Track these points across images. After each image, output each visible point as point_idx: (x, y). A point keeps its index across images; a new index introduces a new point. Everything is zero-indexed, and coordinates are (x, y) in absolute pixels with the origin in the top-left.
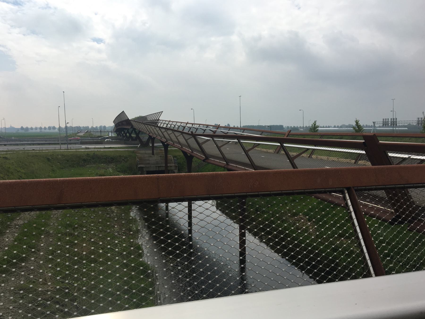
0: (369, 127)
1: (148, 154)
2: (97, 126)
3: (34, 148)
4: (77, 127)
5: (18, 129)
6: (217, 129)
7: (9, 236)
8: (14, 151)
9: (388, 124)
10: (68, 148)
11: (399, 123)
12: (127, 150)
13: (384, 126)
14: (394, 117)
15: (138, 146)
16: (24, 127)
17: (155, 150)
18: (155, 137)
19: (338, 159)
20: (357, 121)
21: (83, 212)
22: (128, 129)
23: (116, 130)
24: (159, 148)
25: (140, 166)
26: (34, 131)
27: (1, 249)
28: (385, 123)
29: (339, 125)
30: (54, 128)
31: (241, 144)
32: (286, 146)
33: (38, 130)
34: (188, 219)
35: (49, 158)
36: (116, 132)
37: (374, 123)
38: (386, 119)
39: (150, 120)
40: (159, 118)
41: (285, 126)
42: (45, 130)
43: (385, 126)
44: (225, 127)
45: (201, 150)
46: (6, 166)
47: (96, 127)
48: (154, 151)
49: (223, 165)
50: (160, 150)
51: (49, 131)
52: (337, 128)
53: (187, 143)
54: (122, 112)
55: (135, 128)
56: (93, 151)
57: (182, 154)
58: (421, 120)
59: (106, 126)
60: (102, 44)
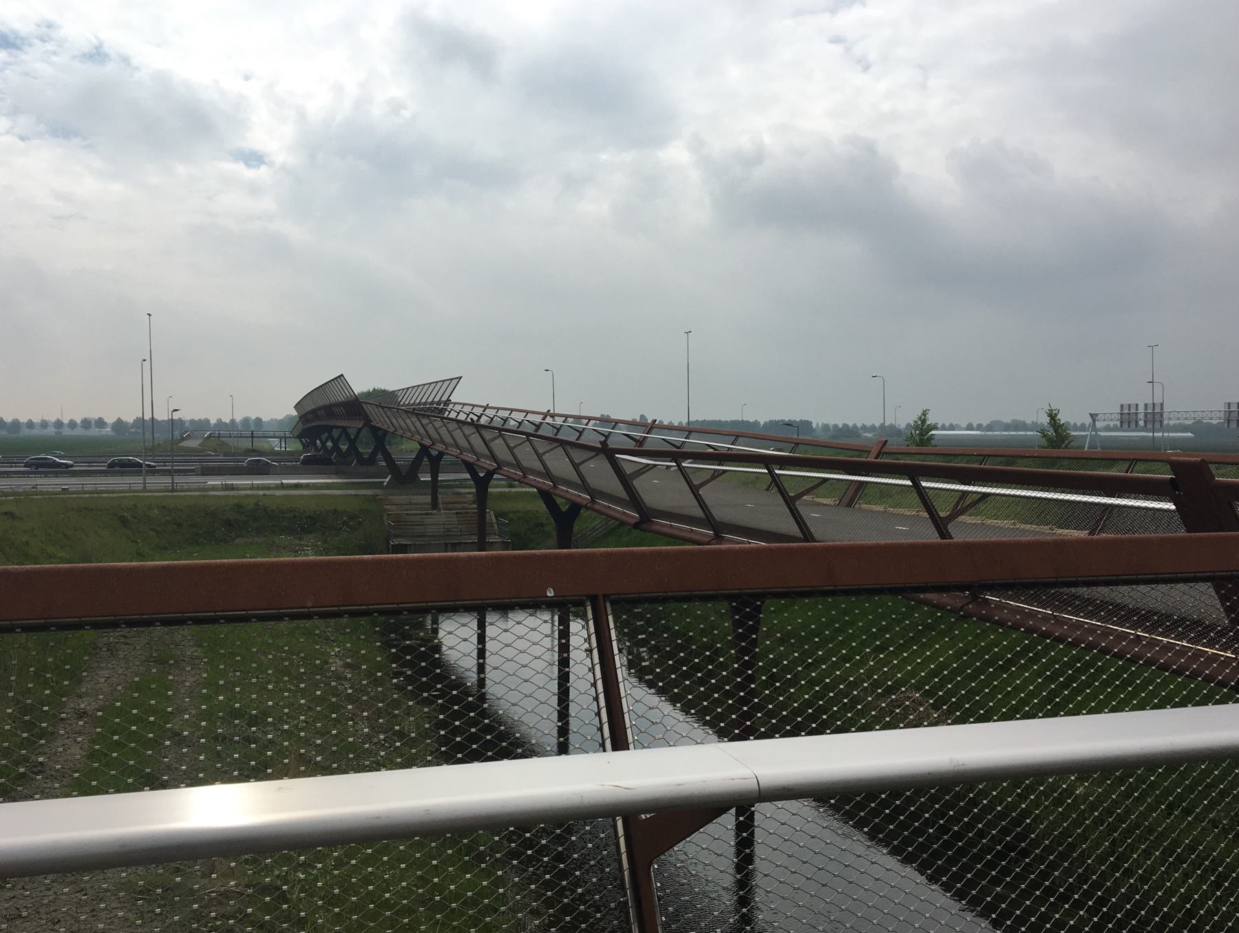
1: (420, 506)
6: (686, 438)
9: (1137, 422)
11: (1170, 419)
12: (353, 492)
13: (1125, 426)
15: (384, 482)
17: (441, 493)
19: (1014, 524)
26: (37, 432)
28: (1127, 418)
29: (1070, 421)
30: (101, 423)
31: (775, 480)
32: (928, 488)
33: (48, 428)
34: (558, 703)
35: (124, 516)
36: (299, 437)
38: (1129, 405)
40: (449, 397)
43: (1127, 427)
45: (628, 499)
48: (440, 496)
51: (71, 433)
52: (977, 430)
53: (578, 474)
57: (541, 506)
58: (1229, 408)
59: (263, 420)
60: (264, 169)
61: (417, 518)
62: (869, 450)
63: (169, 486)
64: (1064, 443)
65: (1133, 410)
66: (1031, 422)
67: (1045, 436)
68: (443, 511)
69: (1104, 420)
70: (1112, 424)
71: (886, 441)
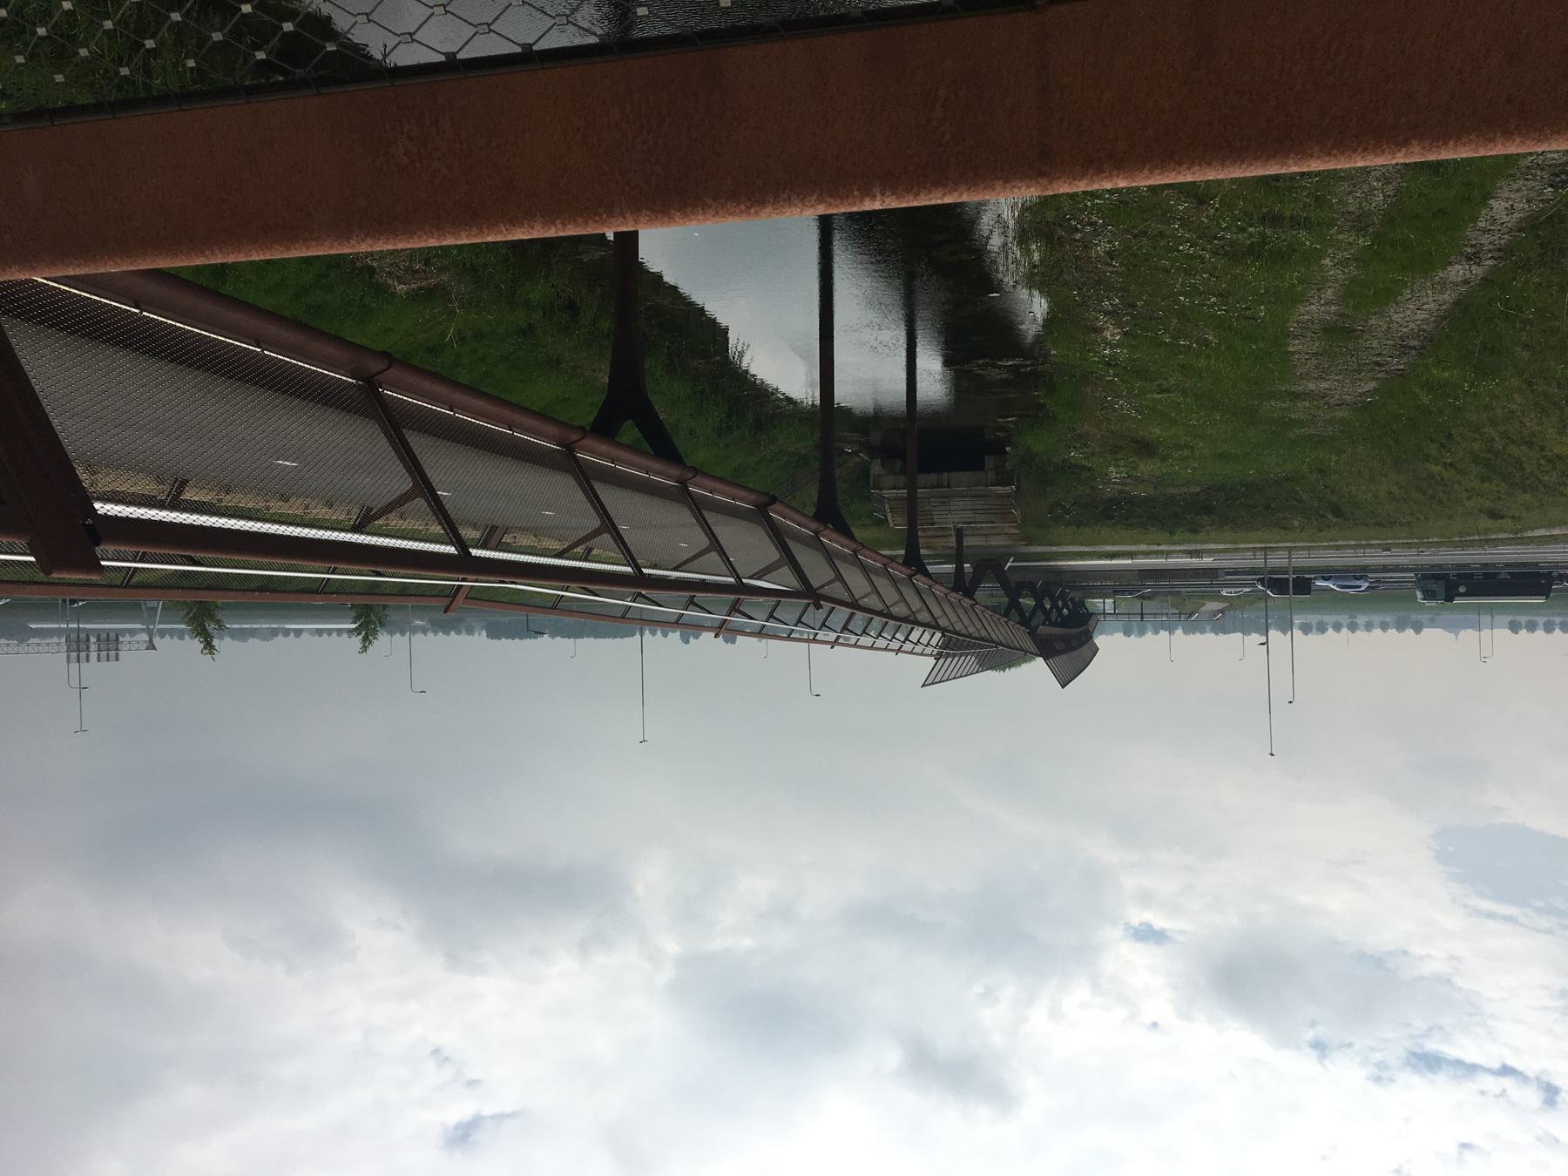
0: (172, 633)
2: (1153, 634)
3: (1385, 556)
4: (1225, 632)
5: (1433, 623)
6: (726, 620)
7: (1507, 215)
8: (1456, 545)
9: (99, 640)
10: (1265, 555)
11: (58, 644)
13: (112, 636)
14: (74, 666)
16: (1410, 632)
17: (952, 547)
18: (953, 594)
20: (210, 650)
21: (1225, 310)
22: (1047, 623)
23: (1090, 623)
24: (938, 556)
25: (1008, 488)
26: (1377, 619)
27: (1540, 163)
28: (110, 645)
30: (1306, 629)
31: (631, 559)
33: (1364, 623)
35: (1337, 517)
37: (151, 646)
38: (108, 660)
39: (968, 654)
41: (481, 638)
42: (1336, 622)
43: (111, 634)
44: (697, 628)
45: (786, 539)
46: (1497, 486)
47: (1156, 632)
48: (955, 545)
49: (698, 479)
50: (935, 549)
54: (1068, 683)
55: (1022, 625)
56: (1174, 544)
57: (856, 532)
59: (1122, 634)
60: (1135, 922)
61: (979, 518)
62: (468, 600)
63: (1270, 555)
64: (195, 613)
65: (104, 654)
66: (225, 639)
67: (218, 622)
68: (952, 526)
69: (138, 642)
70: (128, 638)
71: (445, 612)
